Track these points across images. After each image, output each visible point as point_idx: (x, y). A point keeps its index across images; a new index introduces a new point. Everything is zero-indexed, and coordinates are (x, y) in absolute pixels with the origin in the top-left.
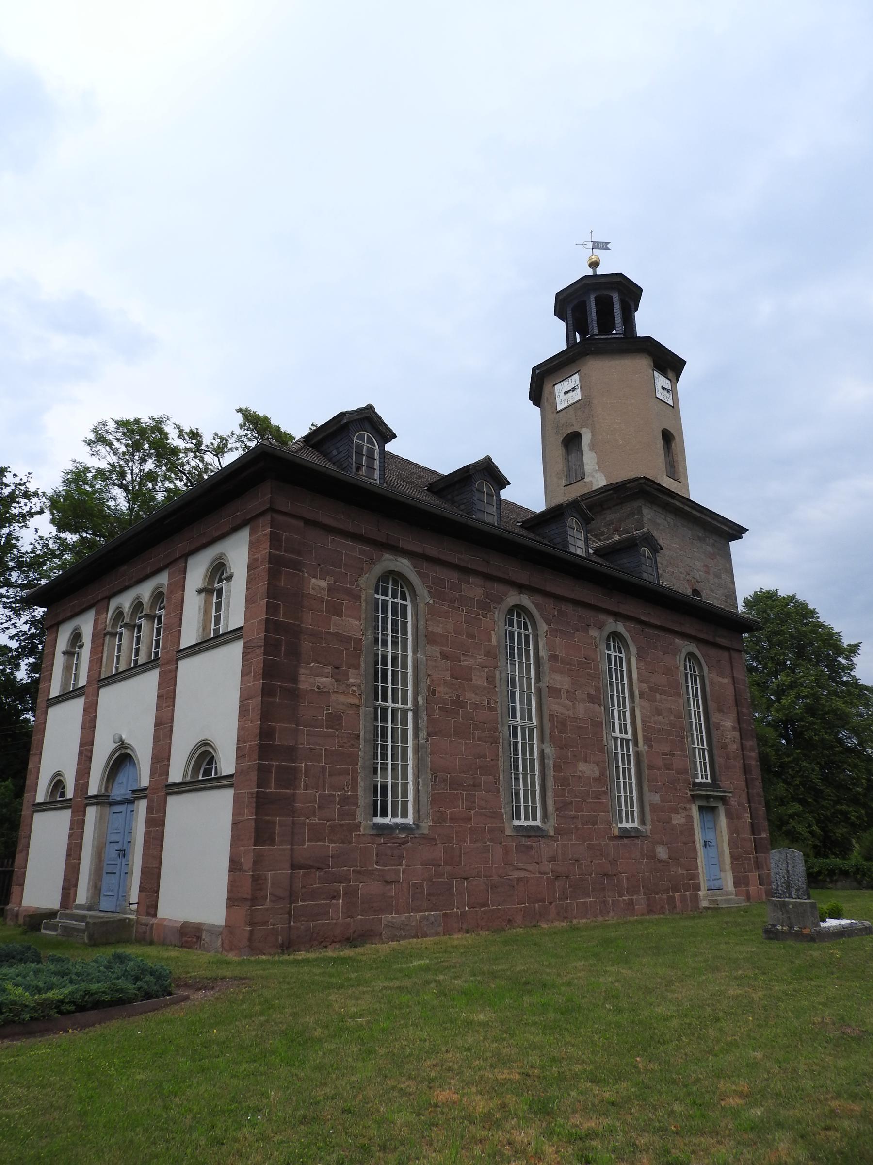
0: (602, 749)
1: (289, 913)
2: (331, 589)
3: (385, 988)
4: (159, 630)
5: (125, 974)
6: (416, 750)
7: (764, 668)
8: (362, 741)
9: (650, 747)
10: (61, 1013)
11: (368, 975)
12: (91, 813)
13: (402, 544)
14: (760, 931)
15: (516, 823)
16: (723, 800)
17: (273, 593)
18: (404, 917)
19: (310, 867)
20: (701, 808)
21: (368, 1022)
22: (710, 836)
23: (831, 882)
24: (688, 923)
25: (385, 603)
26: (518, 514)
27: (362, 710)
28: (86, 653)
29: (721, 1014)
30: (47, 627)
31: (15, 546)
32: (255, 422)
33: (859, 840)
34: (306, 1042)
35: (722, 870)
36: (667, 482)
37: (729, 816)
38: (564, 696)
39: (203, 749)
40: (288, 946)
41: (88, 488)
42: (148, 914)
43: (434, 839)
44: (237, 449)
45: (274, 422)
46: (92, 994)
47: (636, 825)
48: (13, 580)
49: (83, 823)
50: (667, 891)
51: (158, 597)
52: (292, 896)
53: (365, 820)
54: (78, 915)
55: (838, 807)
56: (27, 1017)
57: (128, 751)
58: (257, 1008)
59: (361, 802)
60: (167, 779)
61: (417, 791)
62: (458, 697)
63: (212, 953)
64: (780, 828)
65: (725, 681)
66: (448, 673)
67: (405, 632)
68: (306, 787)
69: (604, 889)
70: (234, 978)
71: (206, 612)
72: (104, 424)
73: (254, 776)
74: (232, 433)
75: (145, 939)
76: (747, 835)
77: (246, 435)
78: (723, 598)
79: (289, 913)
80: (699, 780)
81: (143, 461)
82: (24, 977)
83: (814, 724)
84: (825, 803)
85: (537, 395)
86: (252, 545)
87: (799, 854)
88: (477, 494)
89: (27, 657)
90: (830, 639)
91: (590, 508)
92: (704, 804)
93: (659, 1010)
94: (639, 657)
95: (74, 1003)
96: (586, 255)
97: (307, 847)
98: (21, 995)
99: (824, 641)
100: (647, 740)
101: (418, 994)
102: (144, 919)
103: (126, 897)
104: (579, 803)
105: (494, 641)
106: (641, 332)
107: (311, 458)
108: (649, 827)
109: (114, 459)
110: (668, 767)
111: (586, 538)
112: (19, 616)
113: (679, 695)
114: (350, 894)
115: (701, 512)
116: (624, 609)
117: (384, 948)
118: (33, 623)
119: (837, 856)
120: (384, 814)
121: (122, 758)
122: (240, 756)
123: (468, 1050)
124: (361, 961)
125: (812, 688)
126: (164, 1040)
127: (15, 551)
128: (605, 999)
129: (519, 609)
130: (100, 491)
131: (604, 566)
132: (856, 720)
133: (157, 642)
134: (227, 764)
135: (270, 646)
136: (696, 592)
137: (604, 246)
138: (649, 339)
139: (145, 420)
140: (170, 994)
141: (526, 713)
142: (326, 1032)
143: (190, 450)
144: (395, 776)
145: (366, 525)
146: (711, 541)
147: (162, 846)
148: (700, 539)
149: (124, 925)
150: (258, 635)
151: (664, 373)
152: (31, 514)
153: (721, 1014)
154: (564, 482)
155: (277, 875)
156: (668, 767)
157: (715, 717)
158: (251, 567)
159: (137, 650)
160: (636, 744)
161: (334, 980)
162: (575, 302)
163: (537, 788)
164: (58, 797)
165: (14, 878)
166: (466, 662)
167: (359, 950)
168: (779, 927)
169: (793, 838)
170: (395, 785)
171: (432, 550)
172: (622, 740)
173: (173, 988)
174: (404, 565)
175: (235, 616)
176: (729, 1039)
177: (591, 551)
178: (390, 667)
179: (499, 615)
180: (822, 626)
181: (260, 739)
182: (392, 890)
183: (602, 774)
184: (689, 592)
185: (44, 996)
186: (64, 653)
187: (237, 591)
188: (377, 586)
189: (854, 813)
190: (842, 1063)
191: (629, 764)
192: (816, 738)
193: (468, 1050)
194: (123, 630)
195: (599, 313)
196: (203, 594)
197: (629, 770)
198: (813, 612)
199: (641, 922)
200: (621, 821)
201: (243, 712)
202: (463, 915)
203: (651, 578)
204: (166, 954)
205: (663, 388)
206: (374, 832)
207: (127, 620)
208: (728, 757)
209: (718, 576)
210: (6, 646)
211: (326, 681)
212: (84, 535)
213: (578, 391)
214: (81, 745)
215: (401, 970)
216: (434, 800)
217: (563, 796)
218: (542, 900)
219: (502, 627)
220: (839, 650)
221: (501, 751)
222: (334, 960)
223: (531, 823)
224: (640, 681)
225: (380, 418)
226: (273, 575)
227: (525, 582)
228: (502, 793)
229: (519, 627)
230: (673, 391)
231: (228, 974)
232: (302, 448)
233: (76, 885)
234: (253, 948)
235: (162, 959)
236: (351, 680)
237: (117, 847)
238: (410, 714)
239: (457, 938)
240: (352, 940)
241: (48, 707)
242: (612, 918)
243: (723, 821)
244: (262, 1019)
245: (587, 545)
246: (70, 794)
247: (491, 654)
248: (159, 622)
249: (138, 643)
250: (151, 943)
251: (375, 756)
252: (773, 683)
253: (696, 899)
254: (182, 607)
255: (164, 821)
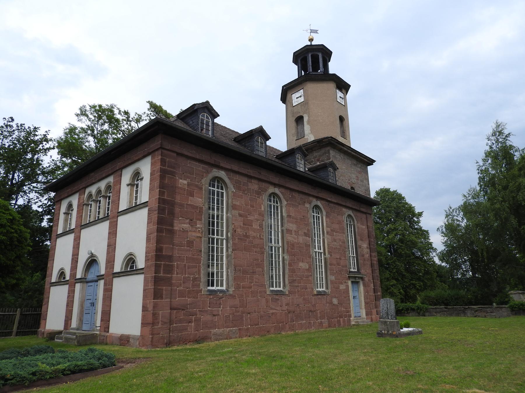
0: (310, 256)
1: (170, 329)
2: (188, 185)
3: (212, 360)
4: (109, 203)
5: (94, 357)
6: (227, 257)
7: (382, 222)
8: (203, 253)
9: (331, 255)
10: (64, 375)
11: (205, 355)
12: (78, 286)
13: (222, 165)
14: (375, 334)
15: (271, 289)
16: (362, 278)
17: (162, 186)
18: (221, 330)
19: (180, 309)
20: (352, 282)
21: (204, 375)
22: (356, 294)
23: (407, 313)
24: (345, 331)
25: (214, 191)
26: (275, 152)
27: (203, 239)
28: (74, 213)
29: (356, 367)
30: (56, 201)
31: (41, 164)
32: (155, 108)
33: (420, 296)
34: (176, 383)
35: (361, 308)
36: (341, 139)
37: (364, 285)
38: (293, 233)
39: (130, 257)
40: (169, 344)
41: (76, 136)
42: (105, 331)
43: (235, 296)
44: (146, 120)
45: (164, 108)
46: (79, 366)
47: (324, 289)
48: (40, 180)
49: (74, 291)
50: (337, 318)
51: (108, 187)
52: (171, 322)
53: (204, 288)
54: (72, 332)
55: (412, 282)
56: (48, 377)
57: (95, 258)
58: (154, 370)
59: (202, 280)
60: (113, 271)
61: (227, 275)
62: (246, 233)
63: (135, 348)
64: (387, 291)
65: (364, 227)
66: (242, 223)
67: (222, 204)
68: (177, 274)
69: (310, 317)
70: (144, 358)
71: (131, 195)
72: (84, 106)
73: (153, 269)
74: (145, 113)
75: (104, 342)
76: (372, 293)
77: (151, 114)
78: (364, 191)
79: (170, 329)
80: (352, 270)
81: (103, 124)
82: (46, 359)
83: (402, 246)
84: (406, 280)
85: (284, 99)
86: (152, 164)
87: (392, 301)
88: (256, 143)
89: (47, 215)
90: (410, 209)
91: (307, 150)
92: (354, 280)
93: (330, 366)
94: (327, 216)
95: (70, 370)
96: (308, 36)
97: (178, 301)
98: (45, 367)
99: (408, 210)
100: (330, 253)
101: (226, 362)
102: (103, 333)
103: (95, 324)
104: (299, 280)
105: (263, 209)
106: (331, 72)
107: (180, 125)
108: (330, 290)
109: (89, 123)
110: (338, 264)
111: (305, 164)
112: (43, 196)
113: (344, 233)
114: (197, 320)
115: (356, 153)
116: (321, 195)
117: (212, 344)
118: (50, 199)
119: (411, 302)
120: (213, 285)
121: (92, 262)
122: (147, 260)
123: (247, 384)
124: (202, 350)
125: (402, 231)
126: (112, 385)
127: (41, 167)
128: (308, 363)
129: (274, 195)
130: (82, 139)
131: (312, 175)
132: (420, 245)
133: (108, 208)
134: (141, 263)
135: (161, 210)
136: (352, 188)
137: (316, 32)
138: (334, 75)
139: (104, 105)
140: (115, 365)
141: (276, 241)
142: (185, 379)
143: (125, 120)
144: (217, 269)
145: (205, 156)
146: (360, 166)
147: (111, 301)
148: (355, 165)
149: (94, 336)
150: (155, 205)
151: (341, 90)
152: (49, 149)
153: (356, 367)
154: (295, 138)
155: (164, 313)
156: (338, 264)
157: (359, 243)
158: (152, 174)
159: (99, 212)
160: (325, 254)
161: (189, 358)
162: (302, 57)
163: (281, 273)
164: (62, 279)
165: (42, 317)
166: (250, 218)
167: (201, 345)
168: (383, 332)
169: (392, 295)
170: (217, 273)
171: (235, 168)
172: (319, 252)
173: (116, 363)
174: (222, 174)
175: (144, 196)
176: (359, 377)
177: (307, 169)
178: (216, 220)
179: (265, 197)
180: (407, 204)
181: (156, 252)
182: (216, 319)
183: (310, 267)
184: (349, 188)
185: (56, 367)
186: (64, 213)
187: (145, 185)
188: (210, 184)
189: (418, 284)
190: (404, 385)
191: (321, 263)
192: (403, 252)
193: (247, 384)
194: (92, 203)
195: (313, 62)
196: (130, 186)
197: (322, 265)
198: (404, 198)
199: (325, 331)
200: (318, 288)
201: (148, 240)
202: (248, 329)
203: (333, 182)
204: (113, 349)
205: (340, 97)
206: (208, 293)
207: (94, 198)
208: (364, 260)
209: (362, 181)
210: (36, 210)
211: (186, 226)
212: (74, 159)
213: (303, 97)
214: (73, 255)
215: (219, 353)
216: (235, 279)
217: (292, 277)
218: (283, 322)
219: (266, 202)
220: (414, 215)
221: (265, 257)
222: (190, 349)
223: (278, 289)
224: (327, 227)
225: (212, 107)
226: (162, 177)
227: (277, 182)
228: (265, 276)
229: (274, 202)
230: (345, 99)
231: (142, 356)
232: (176, 120)
233: (71, 319)
234: (153, 345)
235: (111, 351)
236: (198, 226)
237: (90, 301)
238: (225, 241)
239: (245, 339)
240: (197, 341)
241: (57, 238)
242: (313, 330)
243: (362, 288)
244: (157, 374)
245: (305, 166)
246: (68, 278)
247: (261, 214)
248: (109, 199)
249: (99, 209)
250: (106, 344)
251: (209, 260)
252: (386, 228)
253: (349, 321)
254: (120, 192)
255: (112, 289)
